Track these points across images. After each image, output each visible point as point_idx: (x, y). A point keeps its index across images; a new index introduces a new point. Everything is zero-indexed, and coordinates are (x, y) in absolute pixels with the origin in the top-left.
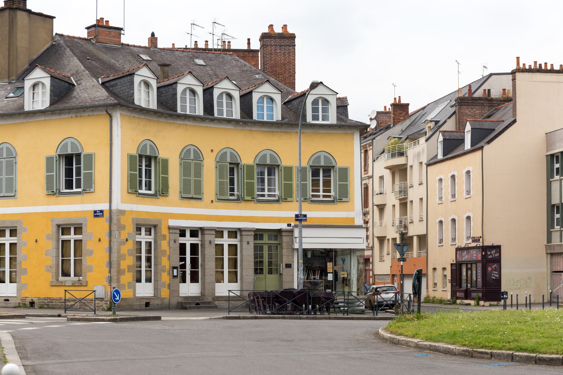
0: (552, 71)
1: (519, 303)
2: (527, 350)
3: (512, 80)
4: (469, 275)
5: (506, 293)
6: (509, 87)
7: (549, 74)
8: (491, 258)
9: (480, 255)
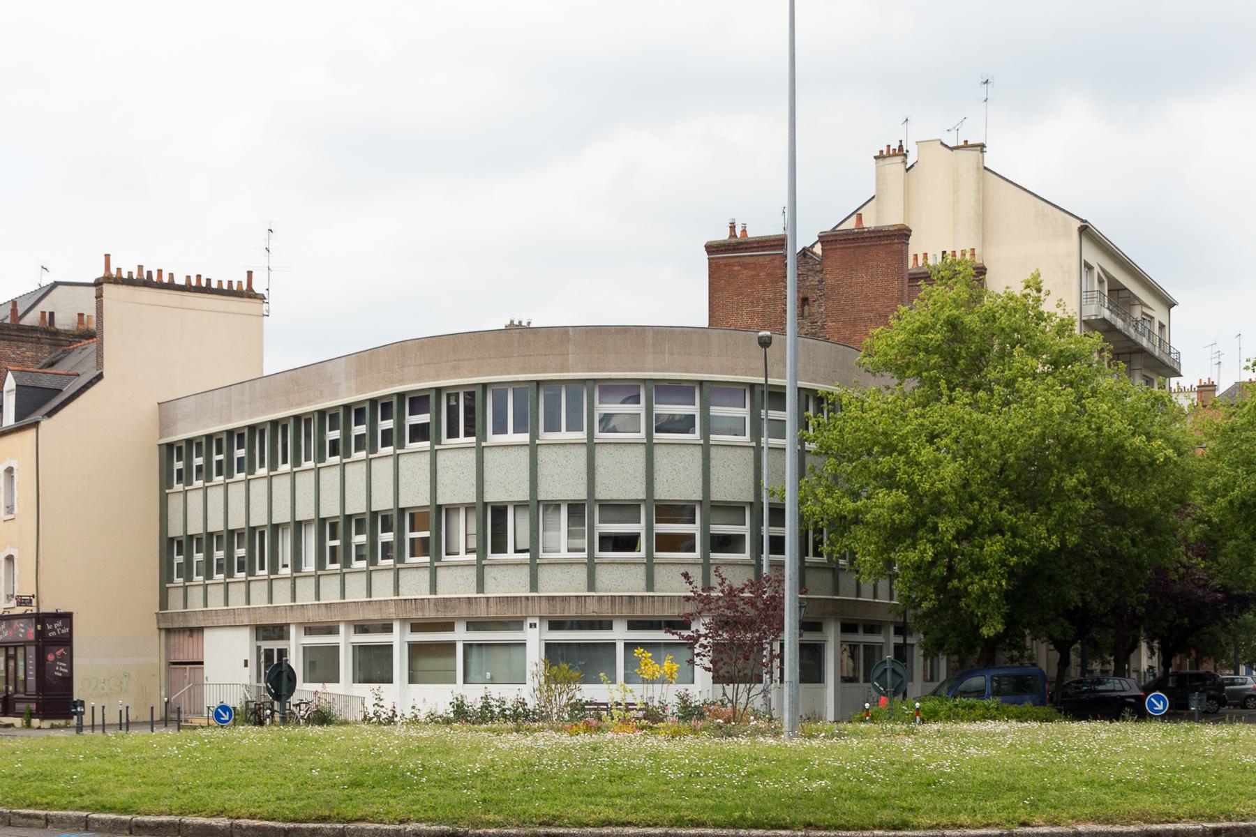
0: (171, 286)
1: (106, 722)
2: (114, 808)
3: (96, 297)
4: (11, 669)
5: (82, 703)
6: (90, 310)
7: (166, 291)
8: (53, 637)
9: (32, 631)
